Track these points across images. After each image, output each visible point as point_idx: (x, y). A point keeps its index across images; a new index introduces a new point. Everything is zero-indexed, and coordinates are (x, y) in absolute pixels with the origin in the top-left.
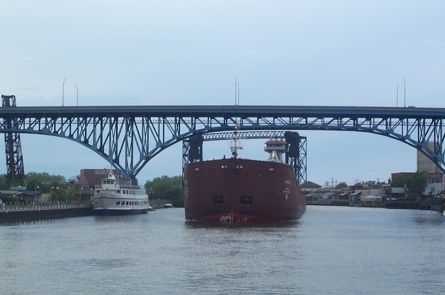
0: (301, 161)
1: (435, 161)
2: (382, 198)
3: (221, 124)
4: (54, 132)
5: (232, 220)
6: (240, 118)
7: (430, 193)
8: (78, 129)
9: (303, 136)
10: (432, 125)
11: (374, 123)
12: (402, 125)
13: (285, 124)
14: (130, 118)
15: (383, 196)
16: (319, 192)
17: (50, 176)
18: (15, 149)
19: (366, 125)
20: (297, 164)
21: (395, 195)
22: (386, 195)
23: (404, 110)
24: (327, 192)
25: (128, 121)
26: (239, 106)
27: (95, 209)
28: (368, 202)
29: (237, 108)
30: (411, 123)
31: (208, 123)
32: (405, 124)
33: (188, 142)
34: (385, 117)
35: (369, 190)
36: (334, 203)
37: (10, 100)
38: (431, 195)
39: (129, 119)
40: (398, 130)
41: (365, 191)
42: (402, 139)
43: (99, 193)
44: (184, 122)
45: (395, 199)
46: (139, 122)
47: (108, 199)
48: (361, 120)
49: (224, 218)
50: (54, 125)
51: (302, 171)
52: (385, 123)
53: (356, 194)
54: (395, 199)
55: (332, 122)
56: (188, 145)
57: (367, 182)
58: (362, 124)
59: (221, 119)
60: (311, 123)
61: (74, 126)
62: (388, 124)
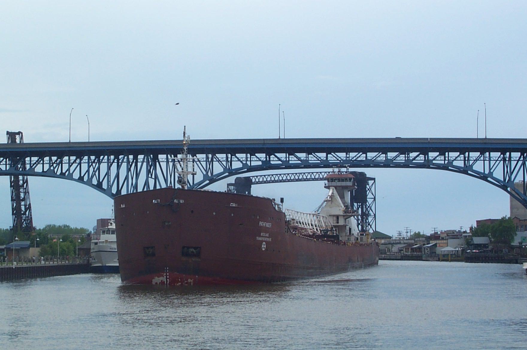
0: (369, 207)
1: (524, 204)
2: (462, 250)
3: (262, 161)
4: (60, 174)
5: (168, 283)
7: (520, 243)
8: (88, 171)
9: (371, 177)
10: (520, 160)
11: (448, 158)
12: (484, 160)
13: (340, 161)
14: (151, 156)
15: (462, 248)
16: (387, 244)
17: (71, 228)
18: (22, 195)
19: (439, 160)
20: (364, 211)
21: (477, 246)
22: (466, 246)
23: (485, 141)
24: (398, 243)
25: (150, 159)
26: (284, 139)
27: (93, 265)
28: (445, 255)
29: (281, 142)
30: (494, 157)
31: (247, 161)
33: (233, 186)
34: (462, 151)
35: (447, 241)
36: (404, 256)
37: (16, 138)
38: (521, 245)
39: (150, 157)
40: (478, 167)
41: (442, 241)
42: (484, 177)
43: (96, 245)
44: (219, 161)
45: (477, 251)
46: (163, 159)
48: (432, 155)
49: (157, 280)
50: (60, 164)
51: (370, 219)
52: (462, 158)
53: (431, 246)
54: (477, 251)
55: (418, 158)
56: (233, 189)
57: (445, 231)
58: (434, 160)
59: (262, 156)
60: (371, 158)
61: (85, 167)
62: (467, 159)
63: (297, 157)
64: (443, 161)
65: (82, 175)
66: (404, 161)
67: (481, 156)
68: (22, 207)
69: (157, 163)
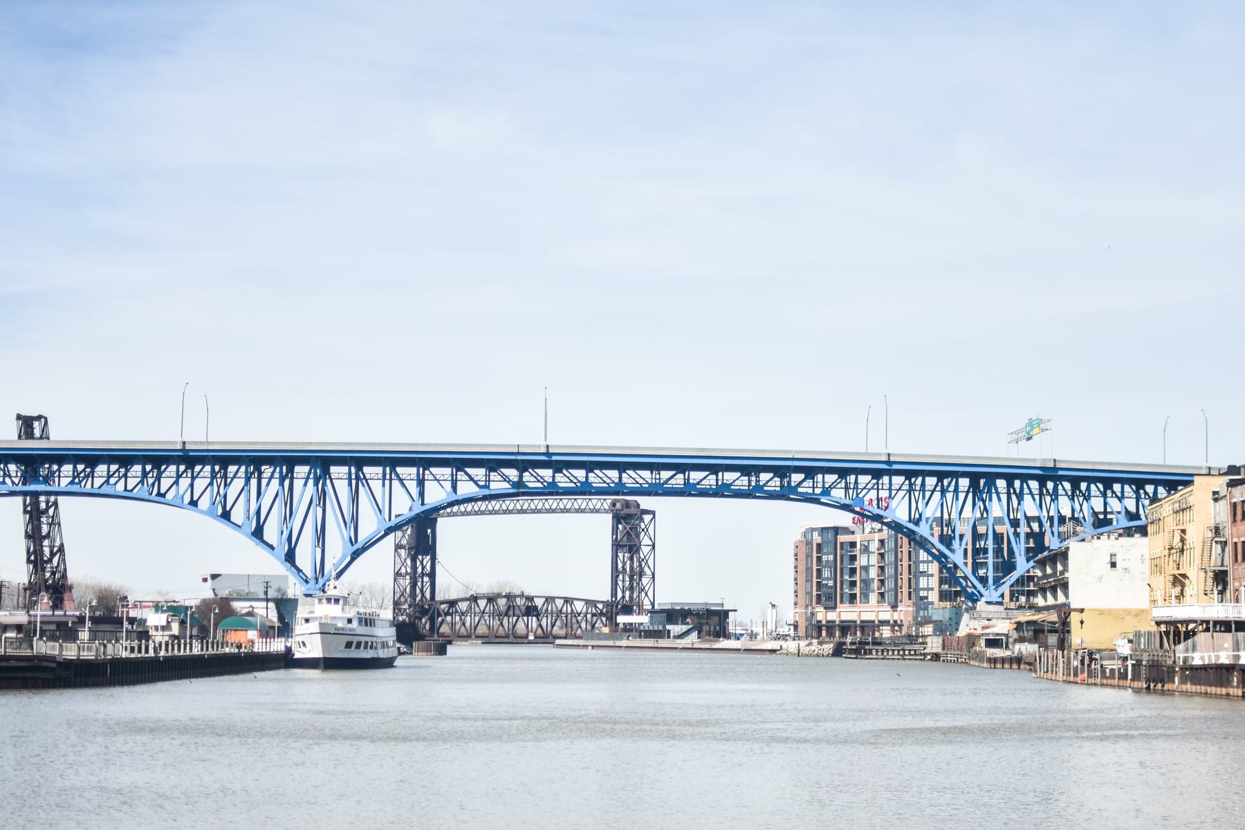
6: (484, 470)
18: (45, 529)
32: (884, 487)
34: (843, 473)
47: (330, 635)
51: (645, 580)
63: (503, 475)
64: (812, 489)
65: (195, 499)
66: (683, 486)
67: (840, 482)
68: (44, 549)
69: (328, 481)
